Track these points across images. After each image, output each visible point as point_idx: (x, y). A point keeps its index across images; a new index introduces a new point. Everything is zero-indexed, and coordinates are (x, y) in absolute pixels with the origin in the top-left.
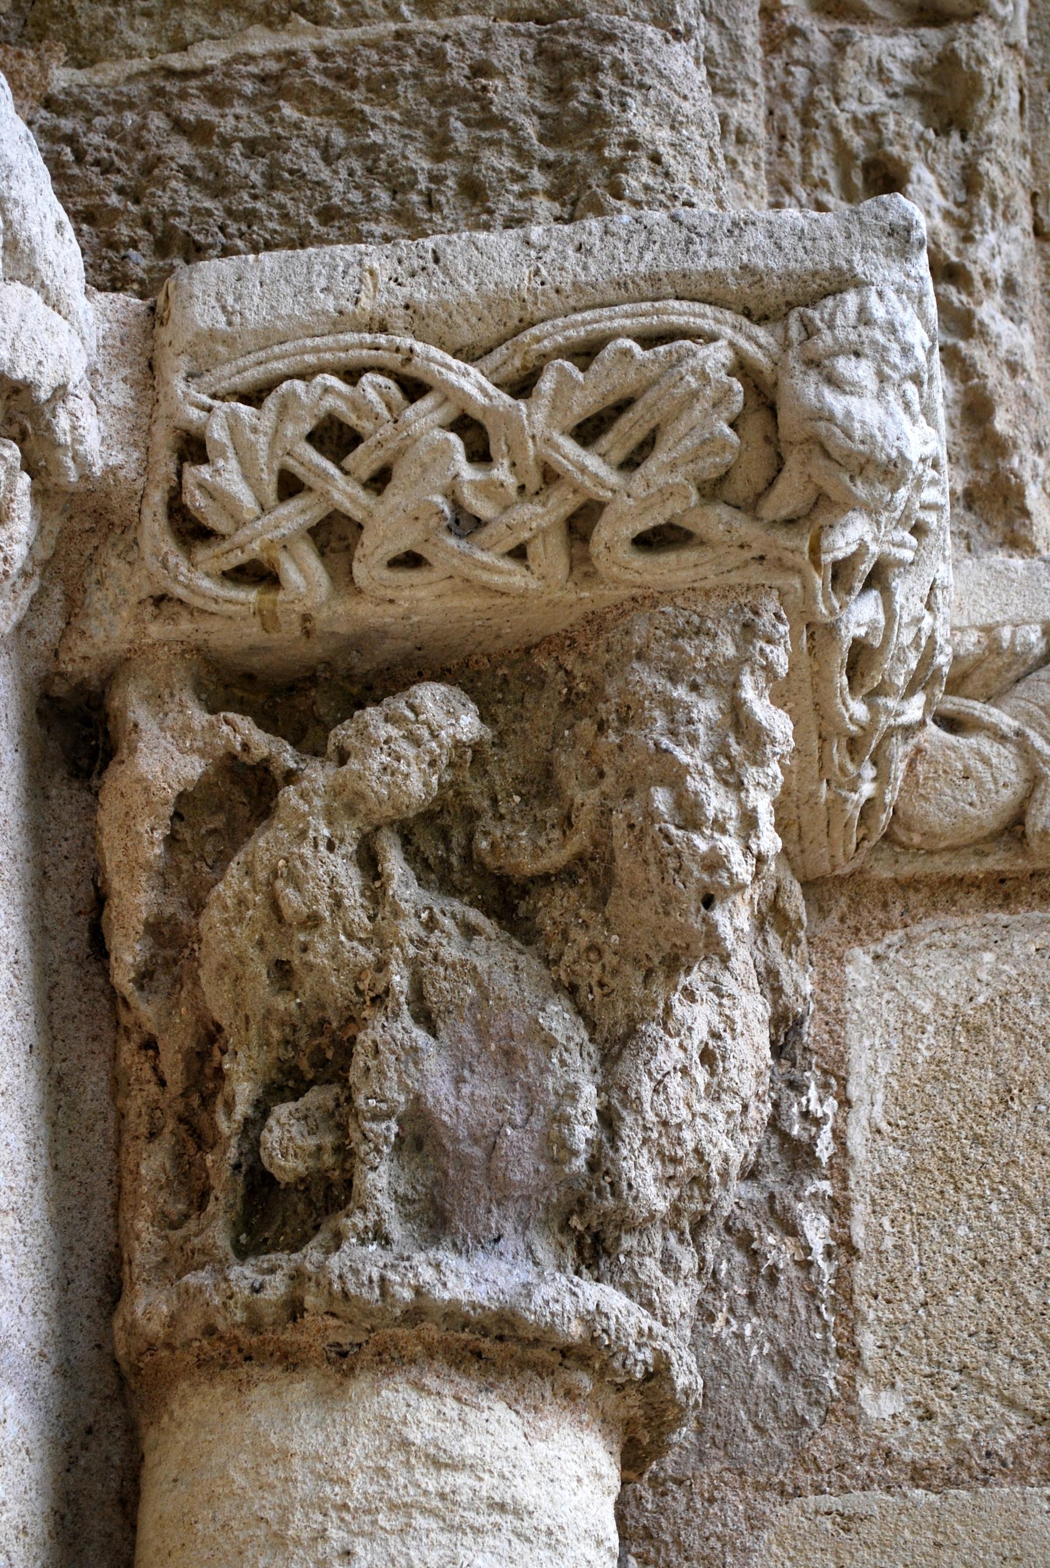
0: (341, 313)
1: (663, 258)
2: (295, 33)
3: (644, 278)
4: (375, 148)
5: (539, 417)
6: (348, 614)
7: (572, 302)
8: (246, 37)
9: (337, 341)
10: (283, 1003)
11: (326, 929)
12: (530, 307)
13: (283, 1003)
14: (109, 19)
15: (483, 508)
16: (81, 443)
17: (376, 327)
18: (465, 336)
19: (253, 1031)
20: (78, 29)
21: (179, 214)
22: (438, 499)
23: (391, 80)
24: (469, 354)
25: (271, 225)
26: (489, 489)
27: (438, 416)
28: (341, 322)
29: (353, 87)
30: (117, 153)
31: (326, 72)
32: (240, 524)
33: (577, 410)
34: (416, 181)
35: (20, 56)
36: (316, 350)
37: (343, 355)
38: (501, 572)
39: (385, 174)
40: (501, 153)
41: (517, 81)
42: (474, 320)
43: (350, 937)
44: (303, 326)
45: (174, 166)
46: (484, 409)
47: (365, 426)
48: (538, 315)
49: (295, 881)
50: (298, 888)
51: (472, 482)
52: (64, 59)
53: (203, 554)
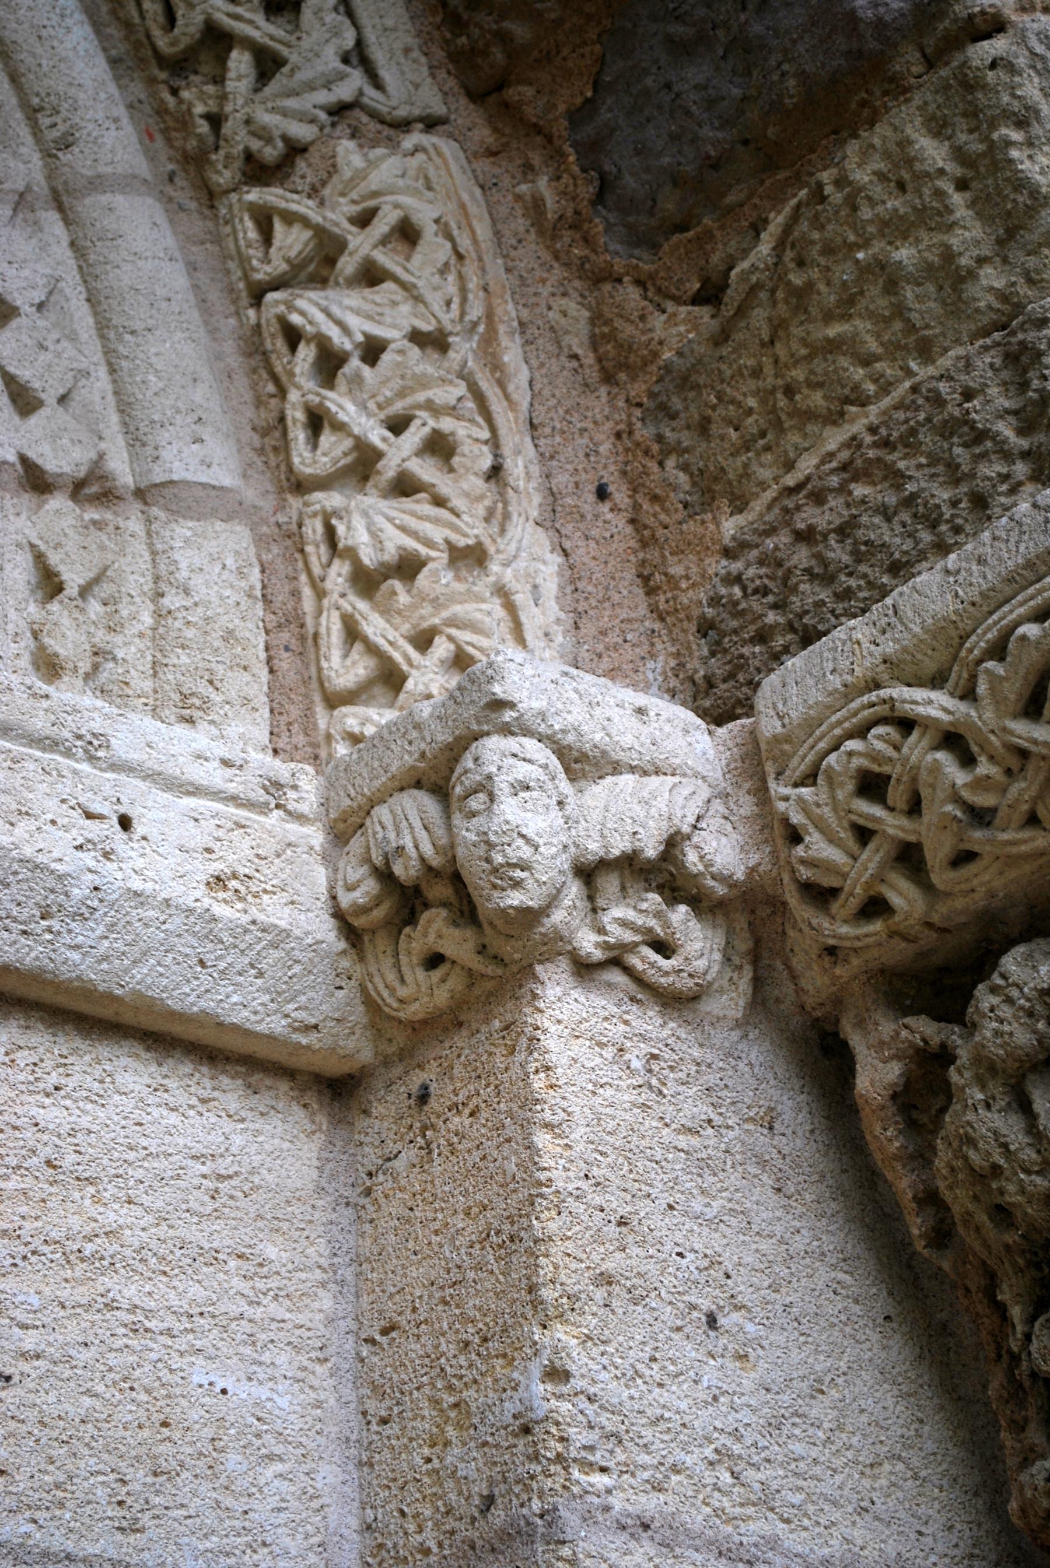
0: (846, 686)
1: (1031, 544)
2: (852, 421)
3: (1024, 568)
4: (913, 496)
5: (989, 715)
6: (846, 961)
7: (985, 609)
8: (824, 440)
9: (878, 696)
10: (1011, 1238)
11: (1007, 1173)
12: (960, 625)
13: (1011, 1238)
14: (746, 466)
15: (984, 800)
16: (712, 865)
17: (872, 686)
18: (930, 666)
19: (1007, 1265)
20: (730, 483)
21: (807, 612)
22: (949, 808)
23: (913, 432)
24: (937, 681)
25: (861, 595)
26: (981, 784)
27: (925, 743)
28: (850, 692)
29: (894, 449)
30: (767, 576)
31: (875, 445)
32: (845, 876)
33: (1012, 697)
34: (942, 514)
35: (703, 522)
36: (839, 723)
37: (854, 720)
38: (1025, 841)
39: (923, 516)
40: (990, 461)
41: (993, 391)
42: (930, 652)
43: (1028, 1172)
44: (828, 707)
45: (798, 572)
46: (951, 723)
47: (886, 769)
48: (968, 628)
49: (971, 1142)
50: (976, 1148)
51: (965, 785)
52: (728, 511)
53: (835, 907)
